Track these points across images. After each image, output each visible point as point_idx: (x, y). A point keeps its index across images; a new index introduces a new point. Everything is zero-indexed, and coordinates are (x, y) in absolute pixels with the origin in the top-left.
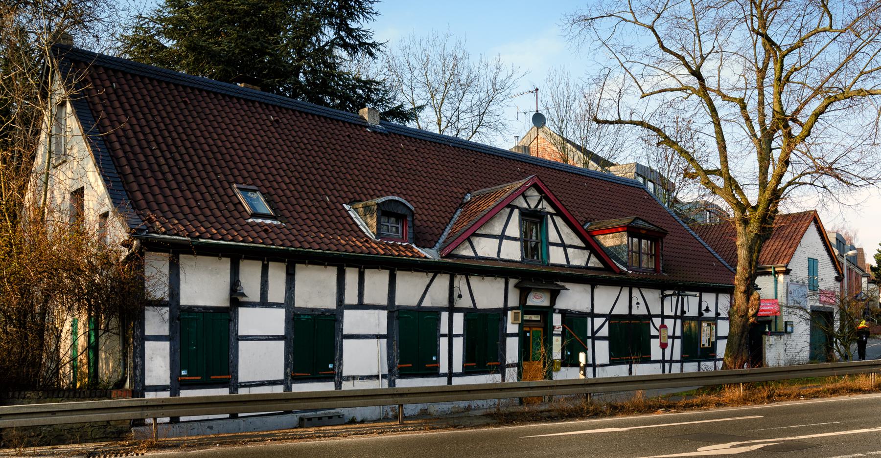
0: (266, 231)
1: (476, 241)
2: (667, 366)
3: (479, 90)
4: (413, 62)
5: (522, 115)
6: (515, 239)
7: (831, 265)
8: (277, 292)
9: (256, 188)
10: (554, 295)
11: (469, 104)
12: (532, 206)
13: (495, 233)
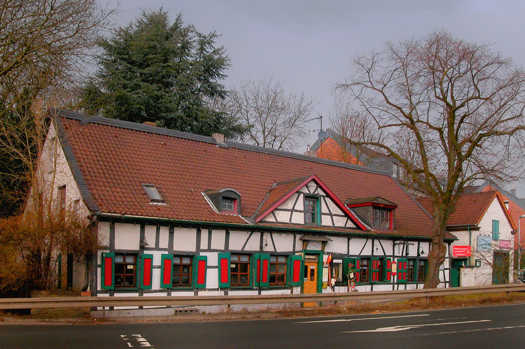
0: (159, 209)
1: (277, 213)
2: (396, 286)
3: (289, 112)
4: (248, 95)
5: (312, 133)
6: (301, 211)
7: (508, 224)
8: (164, 243)
9: (154, 185)
10: (324, 243)
11: (283, 120)
12: (312, 192)
13: (289, 208)
